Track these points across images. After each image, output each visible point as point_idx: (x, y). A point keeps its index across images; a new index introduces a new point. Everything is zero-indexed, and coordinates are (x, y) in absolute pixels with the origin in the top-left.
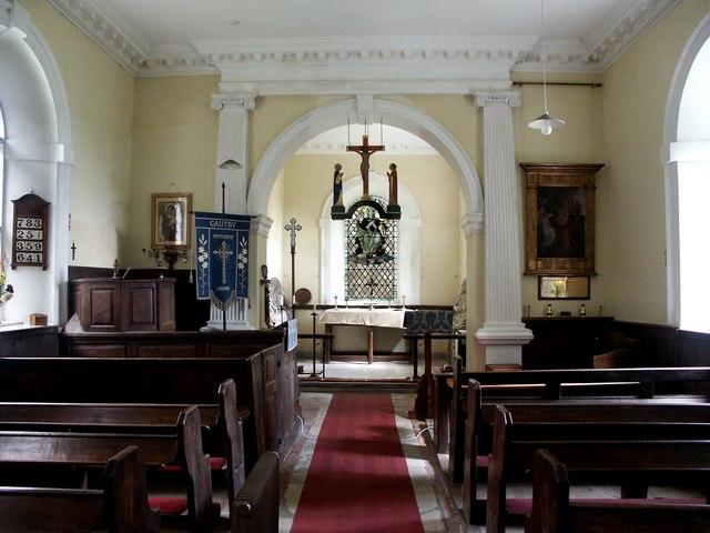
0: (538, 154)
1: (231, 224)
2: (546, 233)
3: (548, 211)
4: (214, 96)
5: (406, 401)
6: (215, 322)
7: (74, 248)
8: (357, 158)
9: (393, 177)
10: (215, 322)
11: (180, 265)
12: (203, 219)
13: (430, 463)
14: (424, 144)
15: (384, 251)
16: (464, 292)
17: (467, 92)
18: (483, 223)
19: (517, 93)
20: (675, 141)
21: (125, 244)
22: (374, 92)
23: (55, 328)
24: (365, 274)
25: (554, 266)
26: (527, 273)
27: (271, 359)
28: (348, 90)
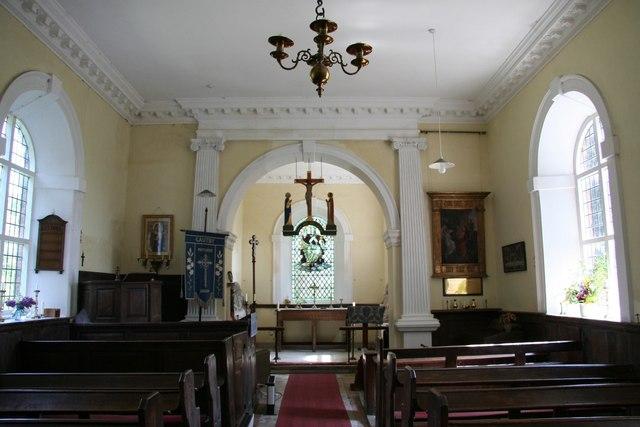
0: (438, 186)
1: (211, 240)
2: (448, 244)
3: (449, 228)
4: (193, 140)
5: (346, 380)
6: (192, 316)
7: (83, 257)
8: (303, 188)
9: (330, 203)
10: (192, 316)
11: (163, 271)
12: (191, 235)
13: (362, 422)
14: (354, 177)
15: (323, 260)
16: (387, 293)
17: (386, 139)
18: (400, 238)
19: (424, 138)
20: (536, 175)
21: (118, 256)
22: (316, 138)
23: (67, 319)
24: (308, 279)
25: (455, 270)
26: (435, 276)
27: (239, 342)
28: (296, 137)
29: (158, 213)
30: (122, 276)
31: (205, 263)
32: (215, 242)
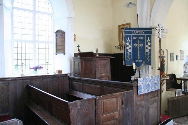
21: (107, 45)
29: (125, 23)
30: (100, 55)
31: (139, 45)
32: (145, 33)
